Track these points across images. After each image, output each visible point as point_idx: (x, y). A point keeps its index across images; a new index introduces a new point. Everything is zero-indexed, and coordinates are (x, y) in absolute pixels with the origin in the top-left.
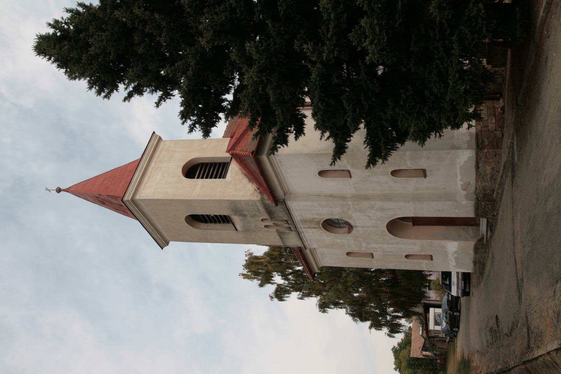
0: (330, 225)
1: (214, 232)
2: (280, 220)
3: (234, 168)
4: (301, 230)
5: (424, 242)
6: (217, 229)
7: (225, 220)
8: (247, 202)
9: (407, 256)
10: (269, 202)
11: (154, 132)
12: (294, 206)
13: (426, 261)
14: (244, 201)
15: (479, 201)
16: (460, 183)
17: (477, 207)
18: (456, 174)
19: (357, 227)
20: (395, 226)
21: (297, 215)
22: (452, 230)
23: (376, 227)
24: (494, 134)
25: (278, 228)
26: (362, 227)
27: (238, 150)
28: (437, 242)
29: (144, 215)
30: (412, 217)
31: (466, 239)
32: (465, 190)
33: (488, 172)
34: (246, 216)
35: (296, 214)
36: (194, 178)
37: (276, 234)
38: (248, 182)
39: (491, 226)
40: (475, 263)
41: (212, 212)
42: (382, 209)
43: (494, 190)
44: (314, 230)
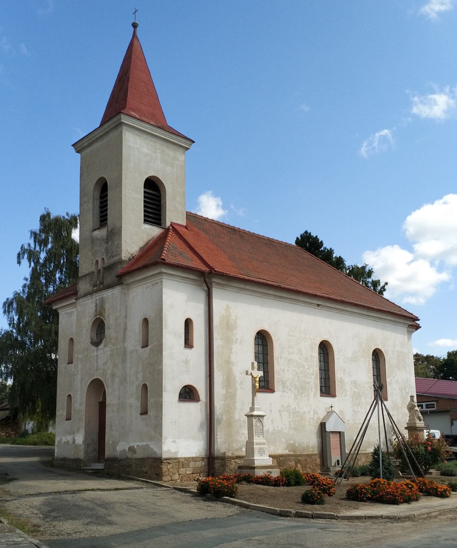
0: (99, 326)
1: (91, 205)
2: (103, 277)
3: (154, 231)
4: (94, 297)
5: (83, 413)
6: (93, 210)
7: (103, 219)
8: (119, 246)
9: (69, 396)
10: (119, 270)
11: (194, 142)
12: (117, 290)
13: (65, 414)
14: (121, 244)
15: (120, 461)
16: (135, 444)
17: (114, 460)
18: (143, 441)
19: (97, 350)
20: (97, 387)
21: (108, 294)
22: (95, 437)
23: (97, 369)
24: (175, 473)
25: (96, 273)
26: (97, 355)
27: (171, 237)
28: (83, 424)
29: (107, 133)
30: (105, 402)
31: (86, 452)
32: (129, 448)
33: (143, 469)
34: (107, 242)
35: (109, 294)
36: (145, 187)
37: (90, 270)
38: (140, 247)
39: (96, 473)
40: (64, 459)
41: (110, 212)
42: (113, 375)
43: (128, 474)
44: (95, 309)
